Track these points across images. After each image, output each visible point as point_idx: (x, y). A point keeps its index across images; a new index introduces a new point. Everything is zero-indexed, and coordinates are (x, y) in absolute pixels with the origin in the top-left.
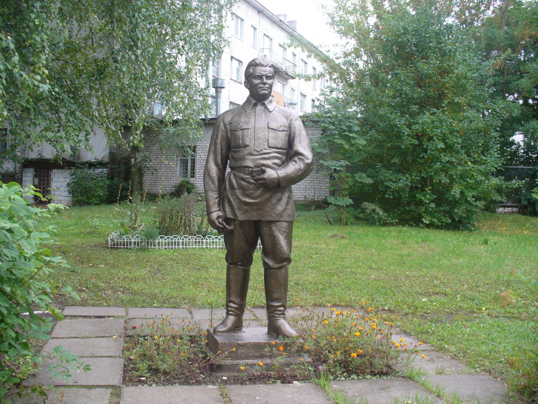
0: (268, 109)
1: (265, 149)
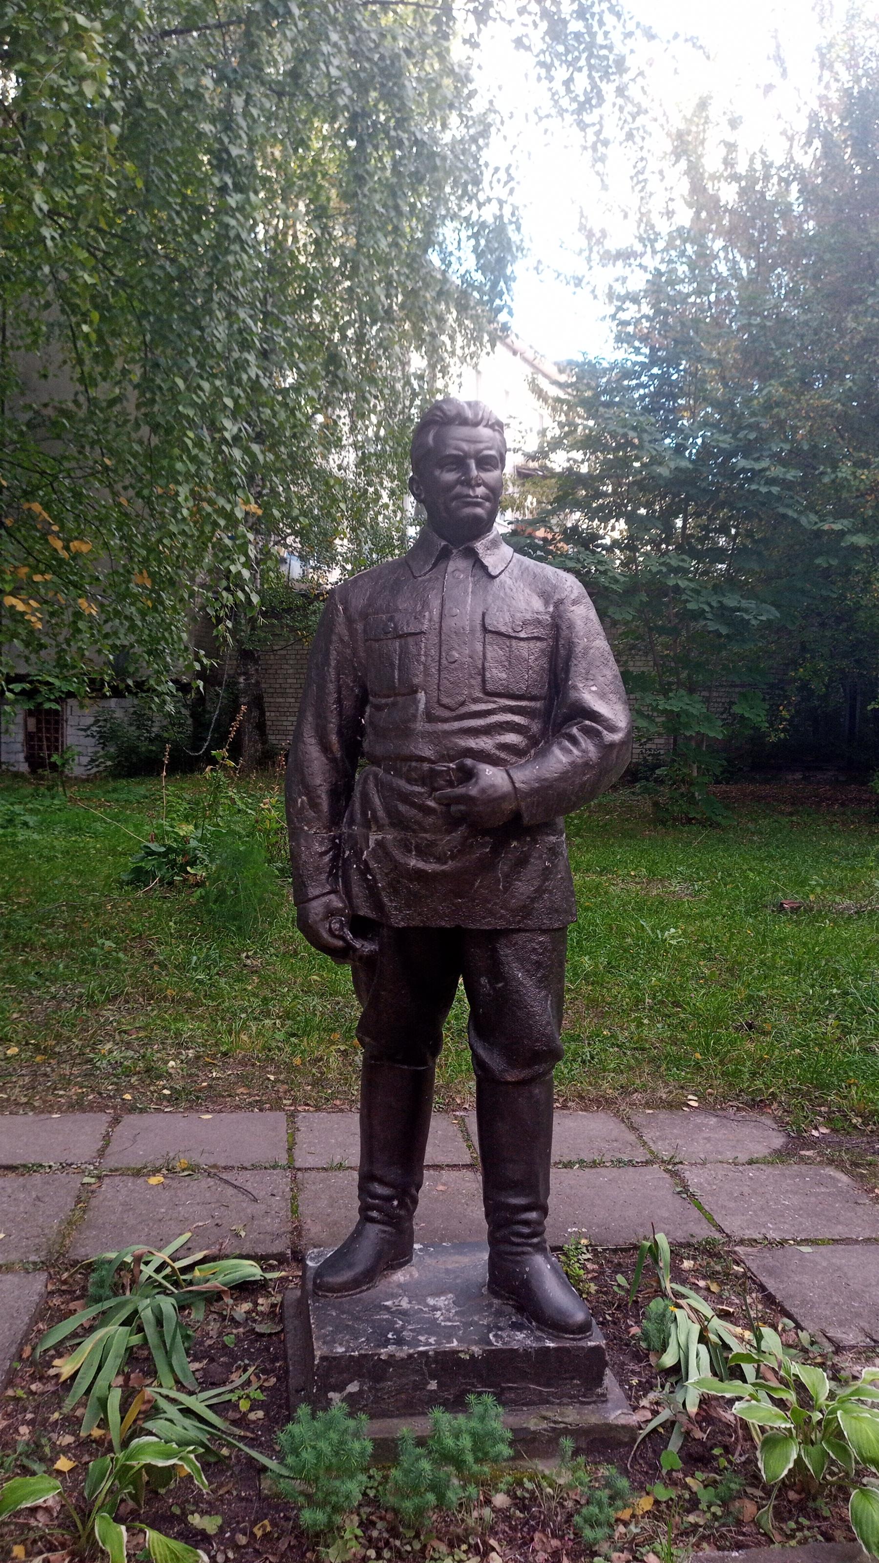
0: (484, 568)
1: (476, 701)
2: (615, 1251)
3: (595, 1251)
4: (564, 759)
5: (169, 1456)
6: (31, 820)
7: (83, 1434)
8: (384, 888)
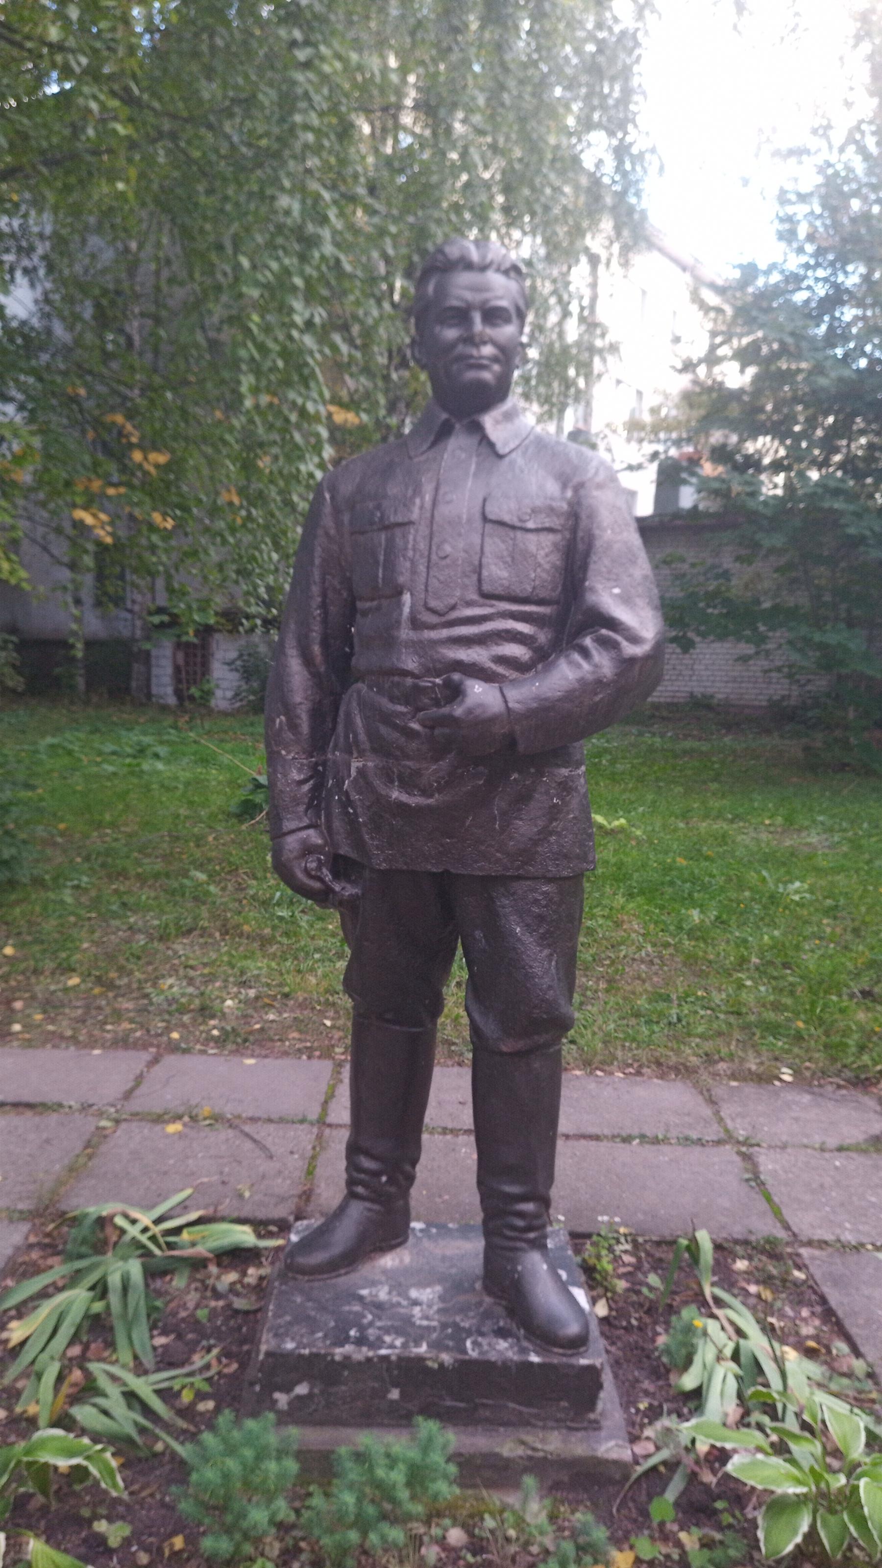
0: (491, 445)
1: (469, 604)
2: (658, 1244)
3: (635, 1242)
5: (72, 1454)
6: (162, 750)
7: (18, 1409)
8: (365, 824)
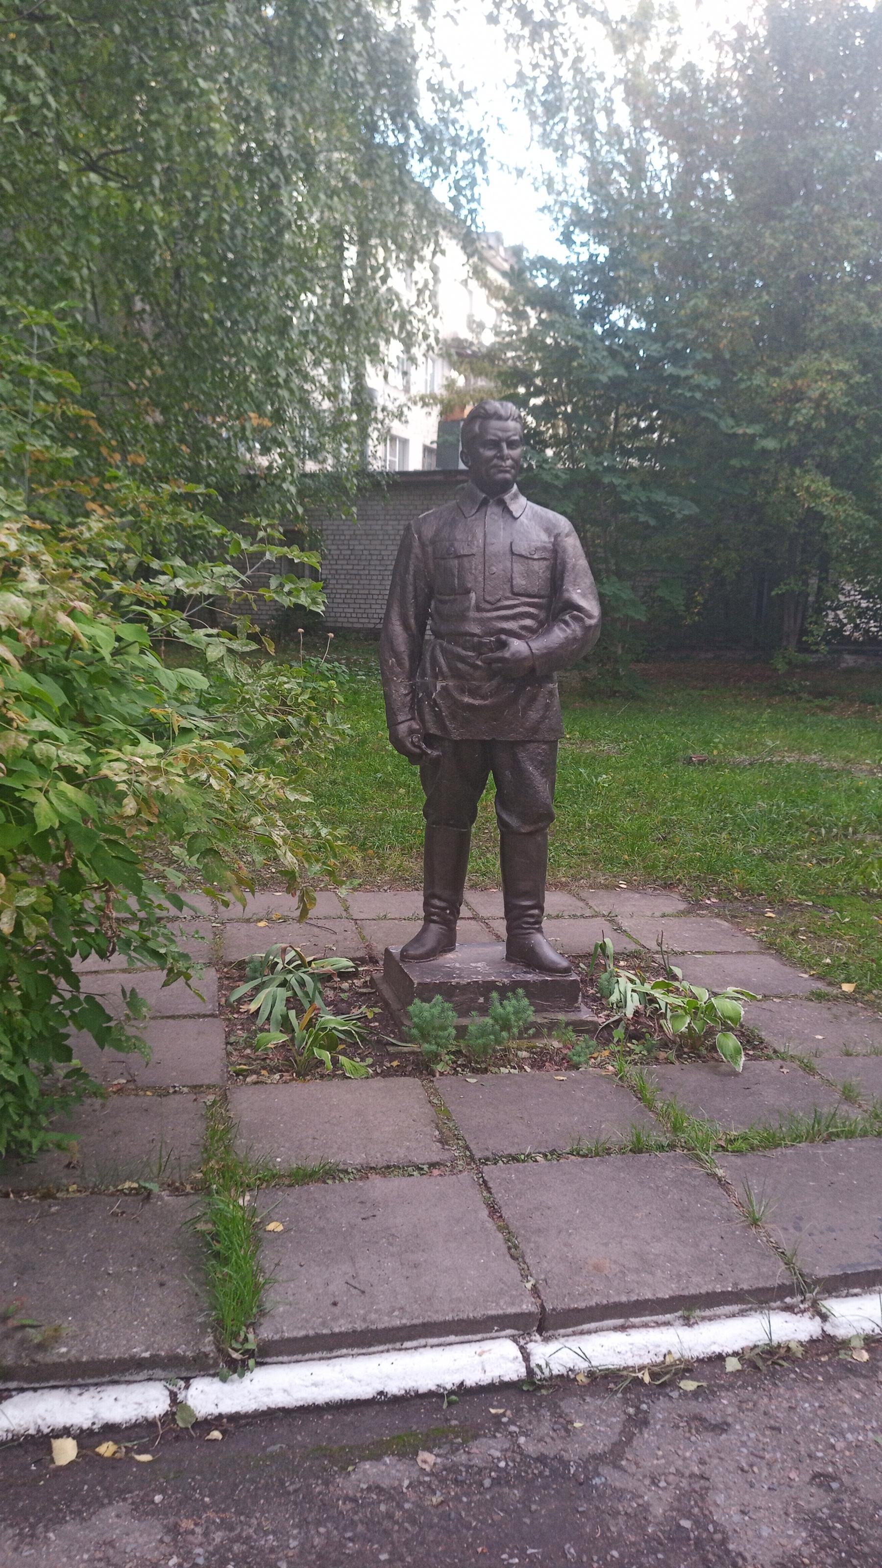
1: (507, 598)
4: (562, 635)
